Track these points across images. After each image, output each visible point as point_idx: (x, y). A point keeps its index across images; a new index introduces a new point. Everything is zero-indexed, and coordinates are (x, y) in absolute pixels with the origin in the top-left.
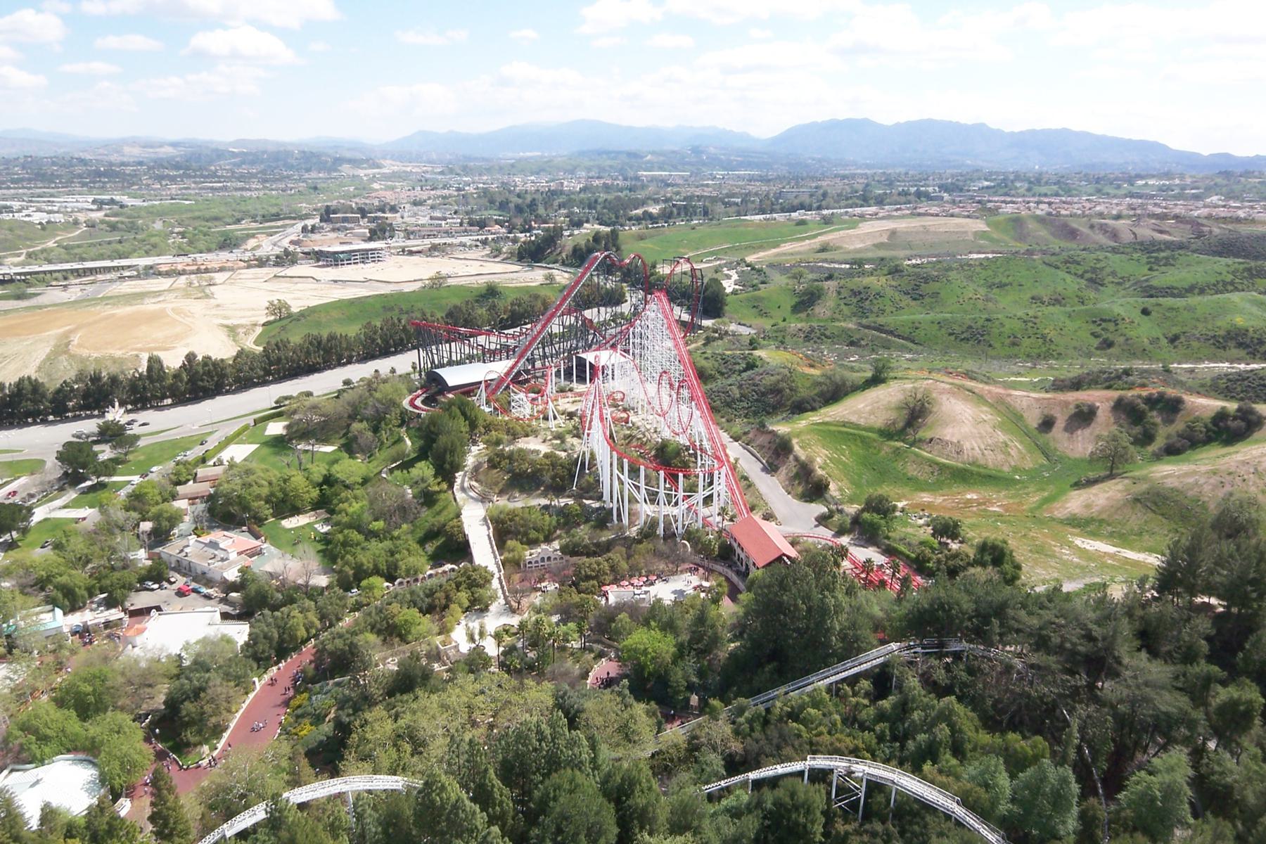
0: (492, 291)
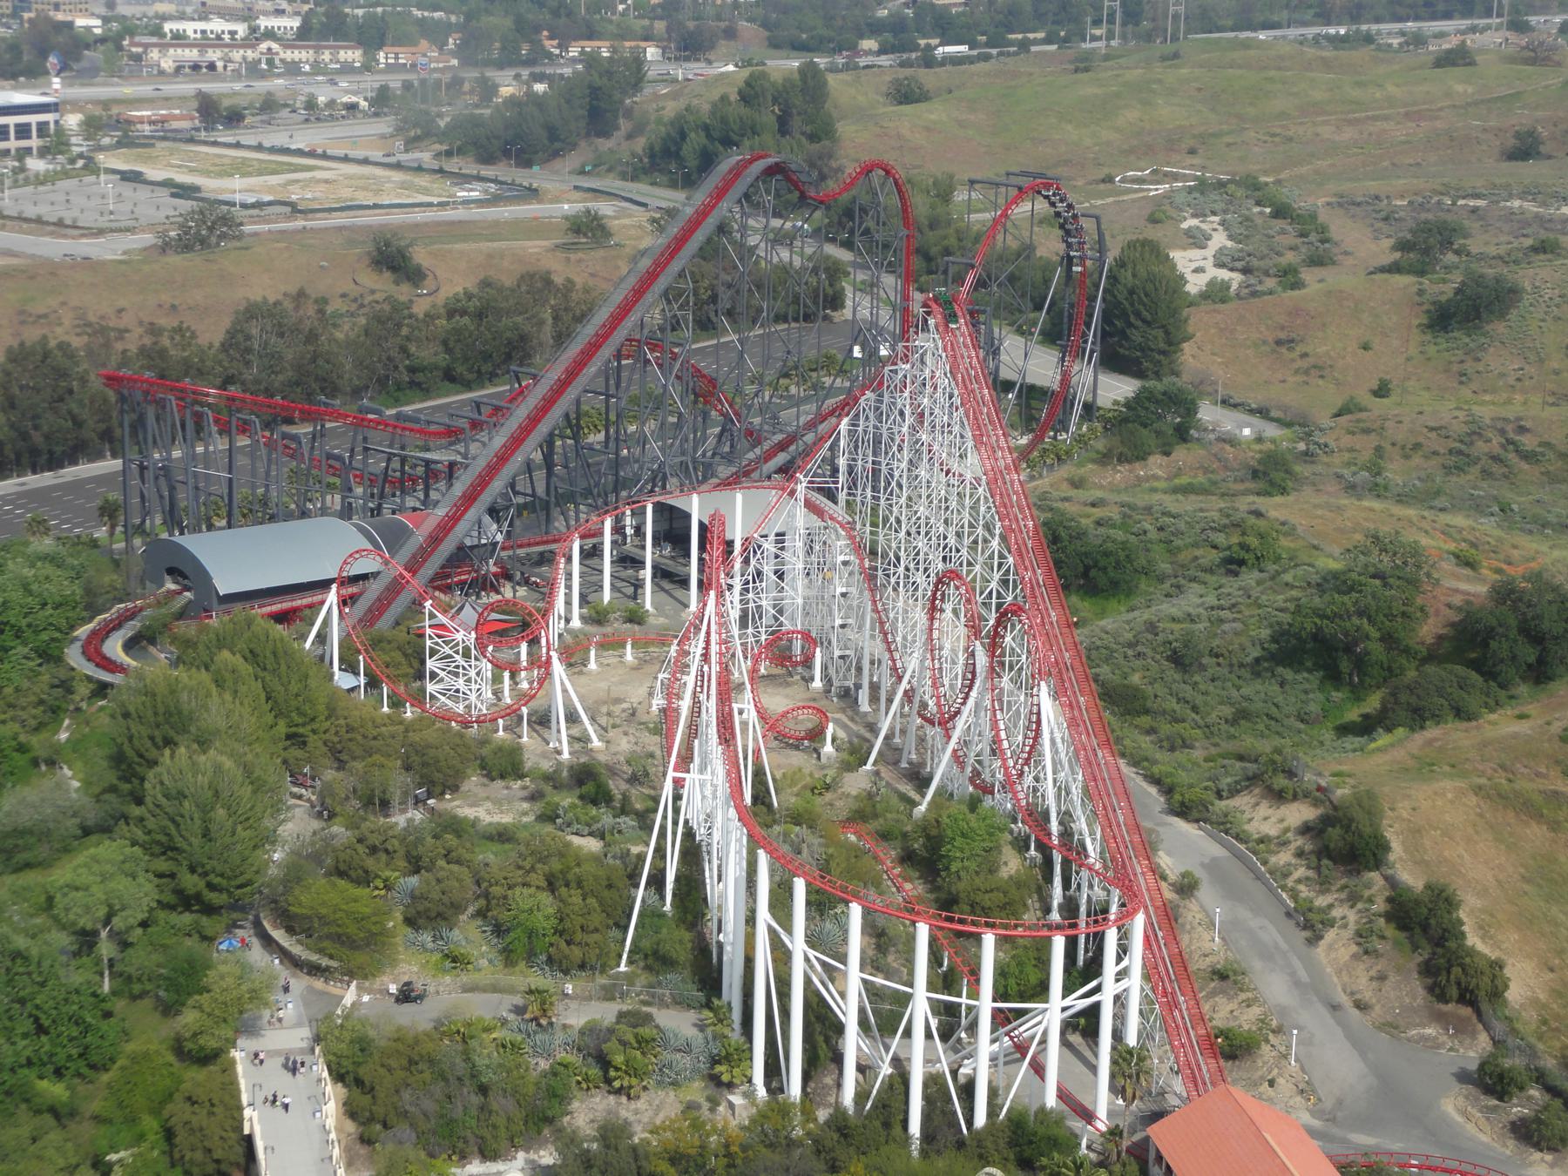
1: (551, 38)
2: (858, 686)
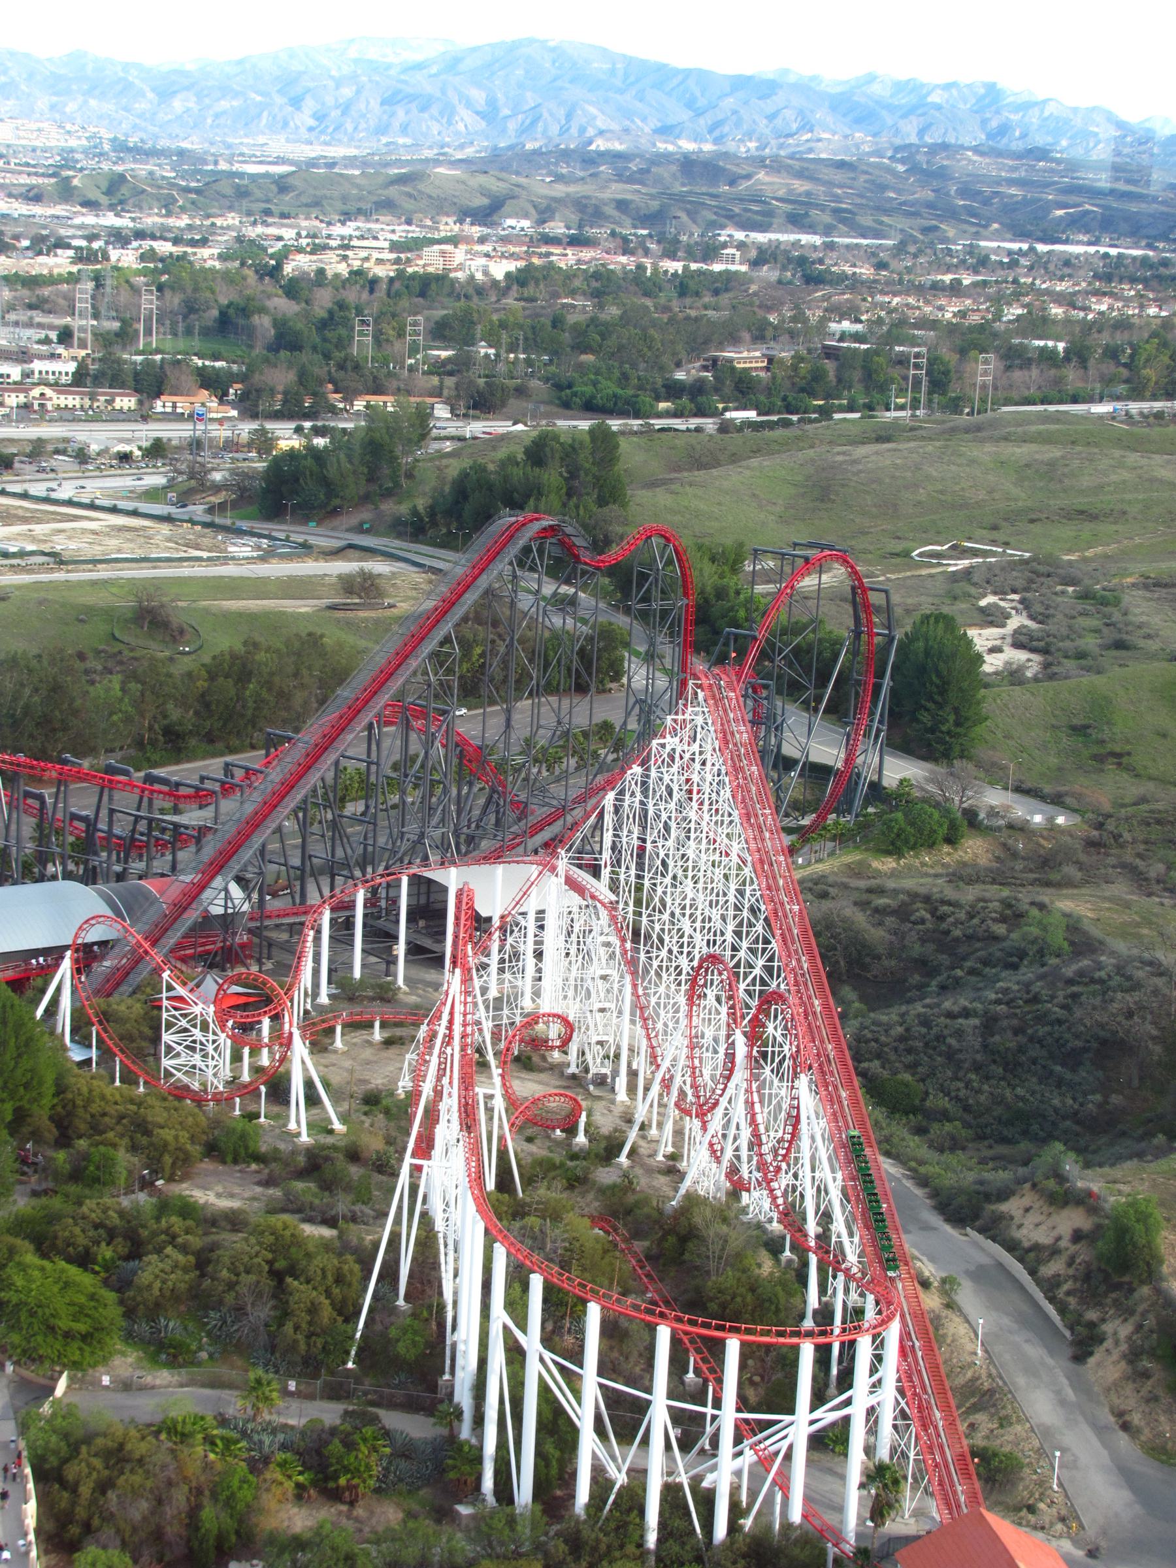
0: (151, 616)
2: (615, 1073)
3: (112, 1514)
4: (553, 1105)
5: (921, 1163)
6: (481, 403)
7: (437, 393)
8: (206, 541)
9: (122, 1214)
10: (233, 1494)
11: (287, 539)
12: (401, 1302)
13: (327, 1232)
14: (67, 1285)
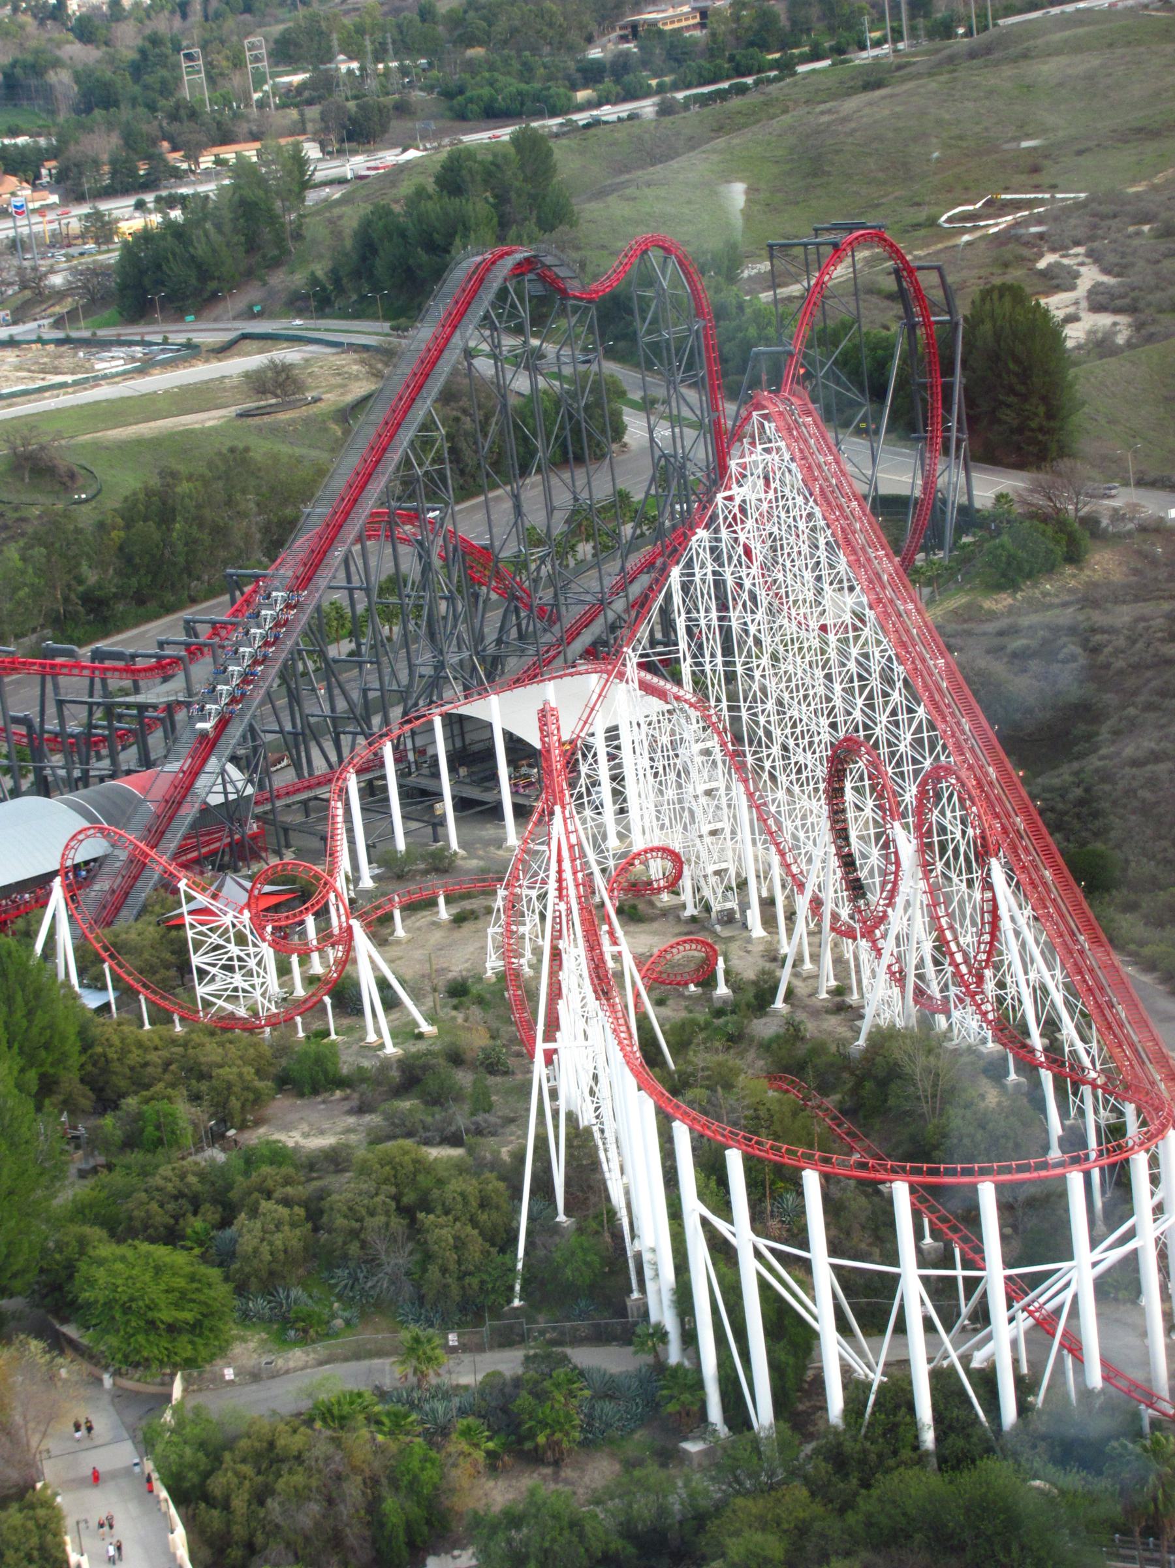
1: (175, 149)
2: (744, 906)
3: (278, 1526)
4: (678, 955)
5: (1142, 944)
6: (357, 132)
7: (300, 128)
8: (66, 362)
9: (202, 1175)
10: (415, 1478)
11: (165, 341)
12: (561, 1217)
13: (457, 1152)
14: (158, 1270)
